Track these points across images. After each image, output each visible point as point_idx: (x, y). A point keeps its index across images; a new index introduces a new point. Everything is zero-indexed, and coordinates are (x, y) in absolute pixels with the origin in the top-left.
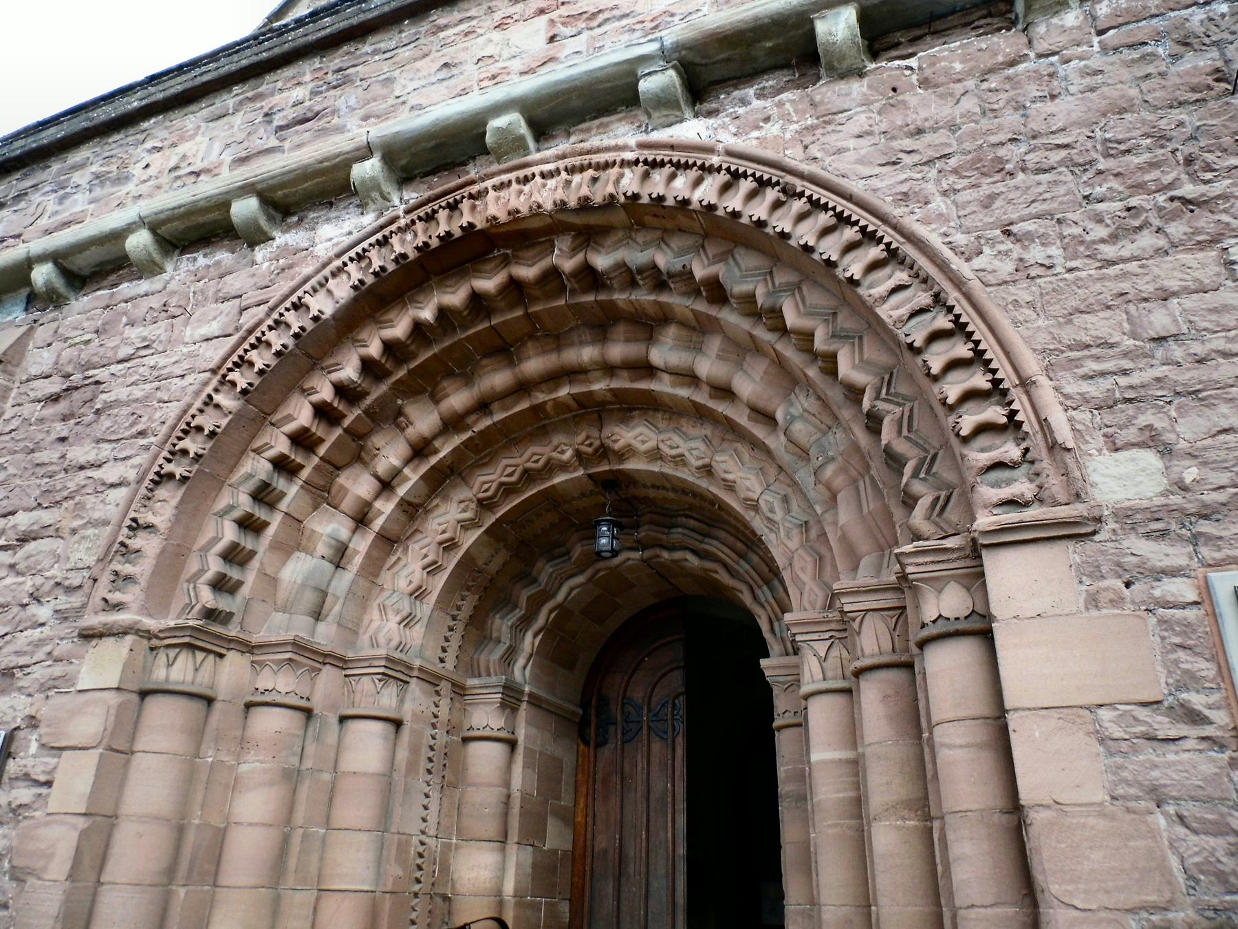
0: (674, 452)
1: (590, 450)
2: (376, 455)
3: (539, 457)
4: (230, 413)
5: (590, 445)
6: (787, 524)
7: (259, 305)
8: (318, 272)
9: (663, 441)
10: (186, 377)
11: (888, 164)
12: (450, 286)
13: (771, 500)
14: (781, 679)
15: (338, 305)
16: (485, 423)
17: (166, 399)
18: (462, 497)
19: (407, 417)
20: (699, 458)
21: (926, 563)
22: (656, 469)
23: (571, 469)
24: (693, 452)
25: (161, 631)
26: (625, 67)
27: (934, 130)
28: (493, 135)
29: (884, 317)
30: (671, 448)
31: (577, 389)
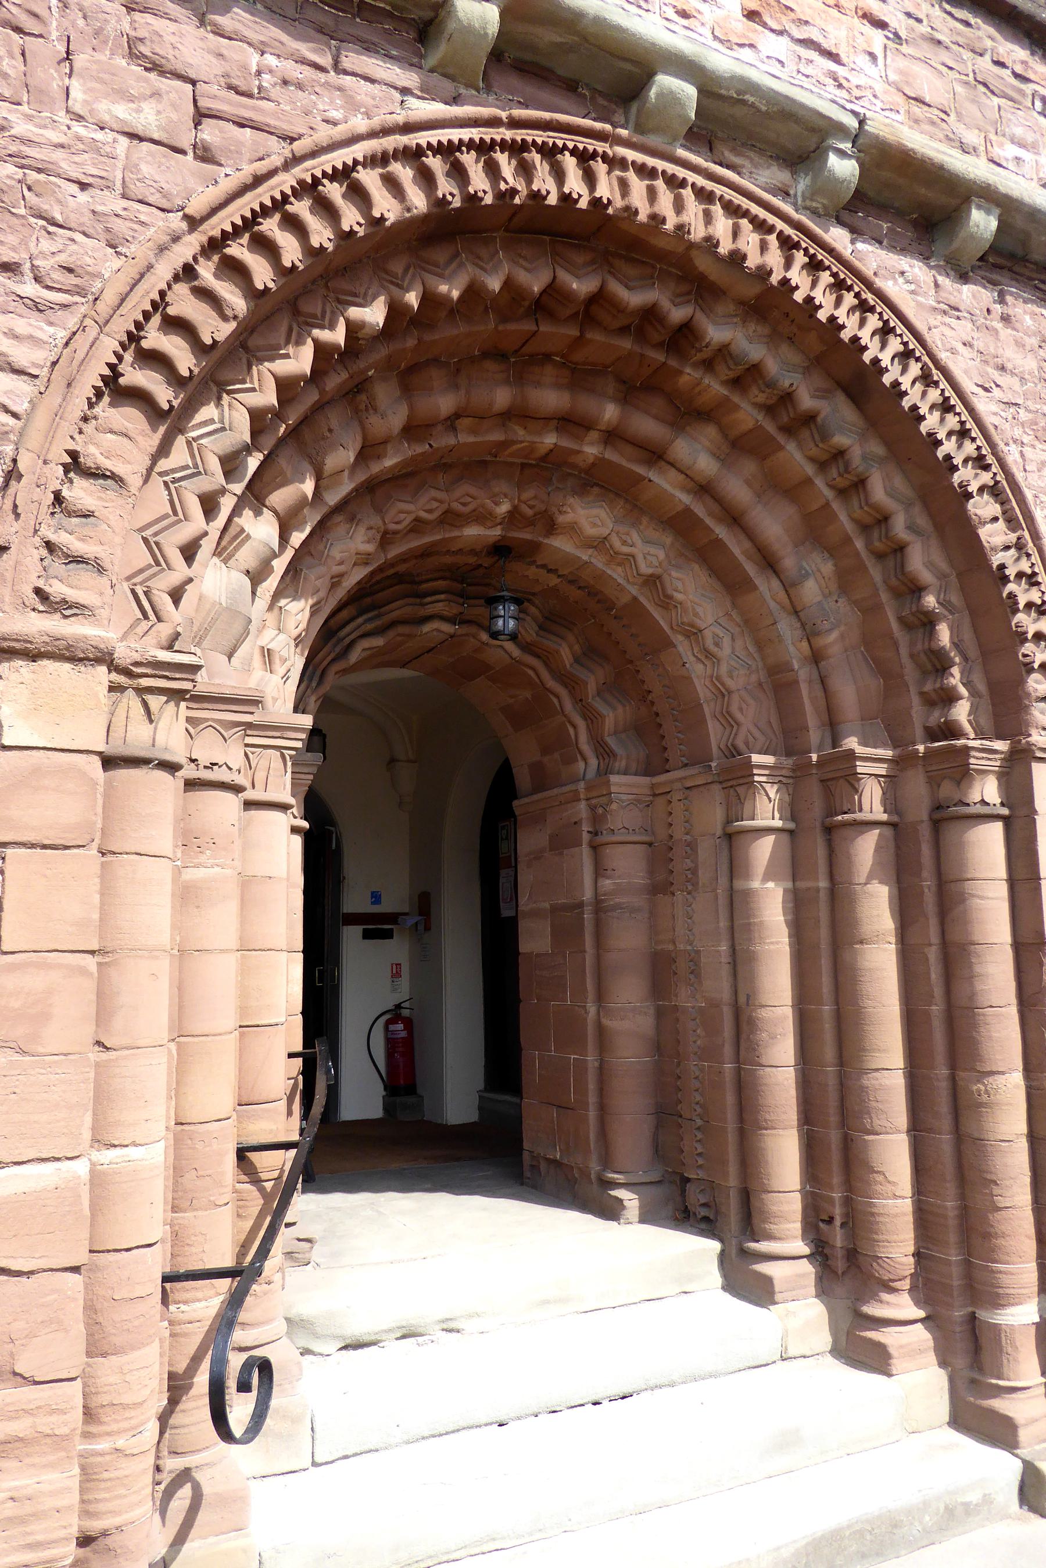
0: (626, 549)
1: (529, 512)
2: (324, 438)
3: (470, 500)
4: (235, 317)
5: (531, 507)
6: (733, 663)
7: (242, 126)
8: (372, 134)
9: (617, 533)
10: (91, 191)
11: (981, 386)
12: (525, 258)
13: (721, 635)
14: (624, 797)
15: (407, 215)
16: (449, 440)
17: (59, 218)
18: (372, 523)
19: (372, 399)
20: (650, 566)
21: (983, 758)
22: (585, 558)
23: (489, 524)
24: (648, 557)
25: (137, 664)
26: (822, 123)
27: (1013, 374)
28: (659, 95)
29: (983, 538)
30: (624, 543)
31: (566, 443)
